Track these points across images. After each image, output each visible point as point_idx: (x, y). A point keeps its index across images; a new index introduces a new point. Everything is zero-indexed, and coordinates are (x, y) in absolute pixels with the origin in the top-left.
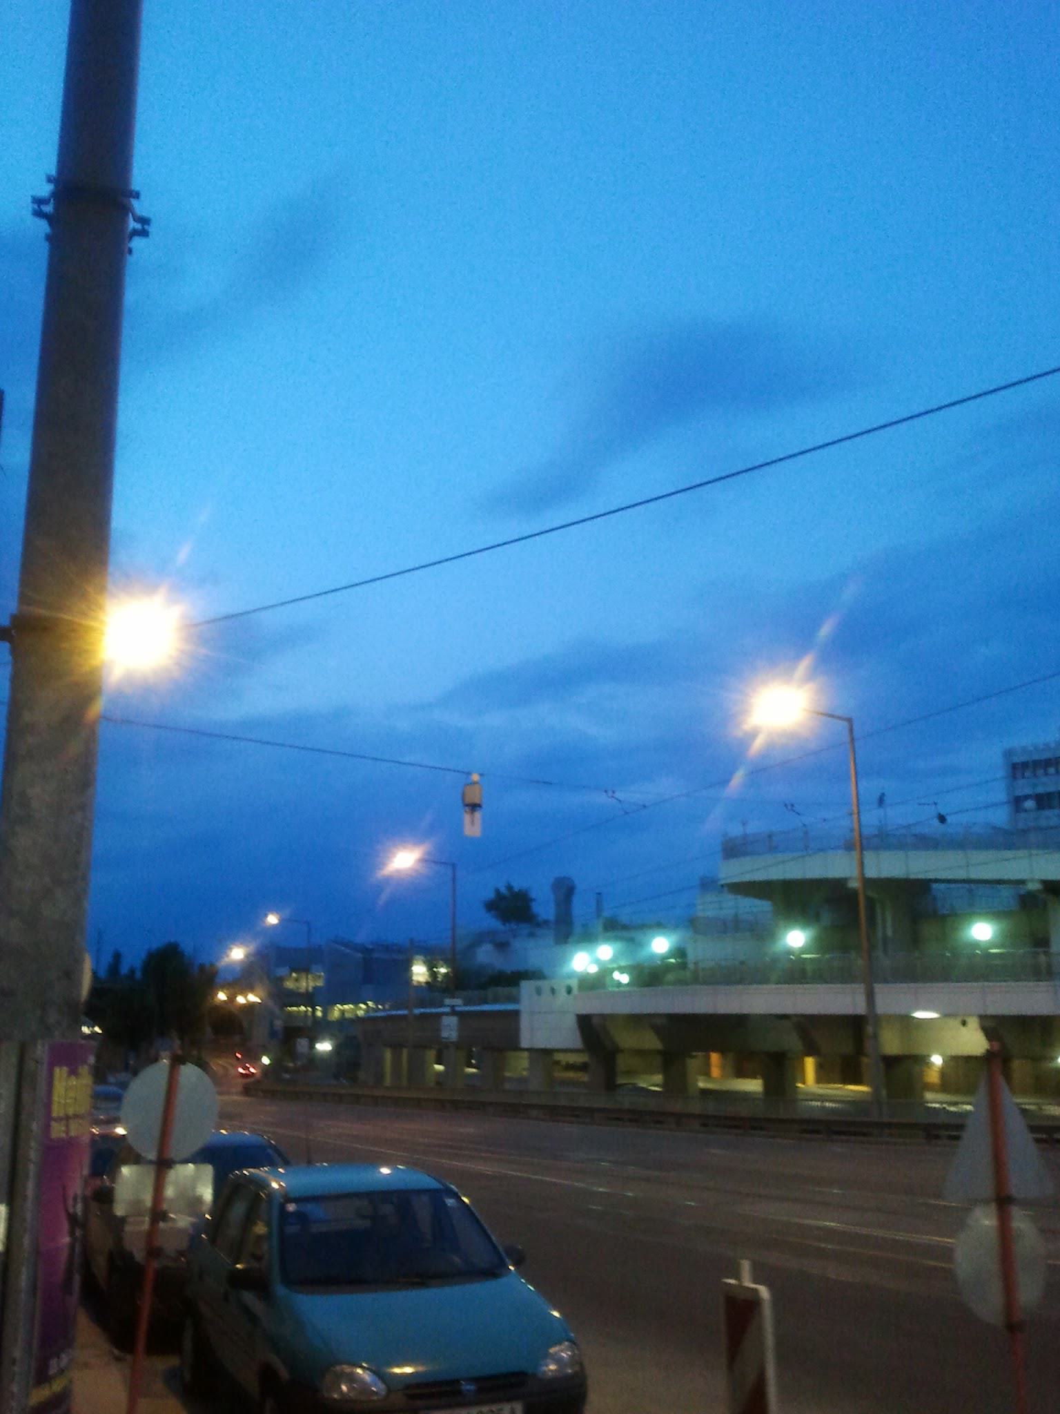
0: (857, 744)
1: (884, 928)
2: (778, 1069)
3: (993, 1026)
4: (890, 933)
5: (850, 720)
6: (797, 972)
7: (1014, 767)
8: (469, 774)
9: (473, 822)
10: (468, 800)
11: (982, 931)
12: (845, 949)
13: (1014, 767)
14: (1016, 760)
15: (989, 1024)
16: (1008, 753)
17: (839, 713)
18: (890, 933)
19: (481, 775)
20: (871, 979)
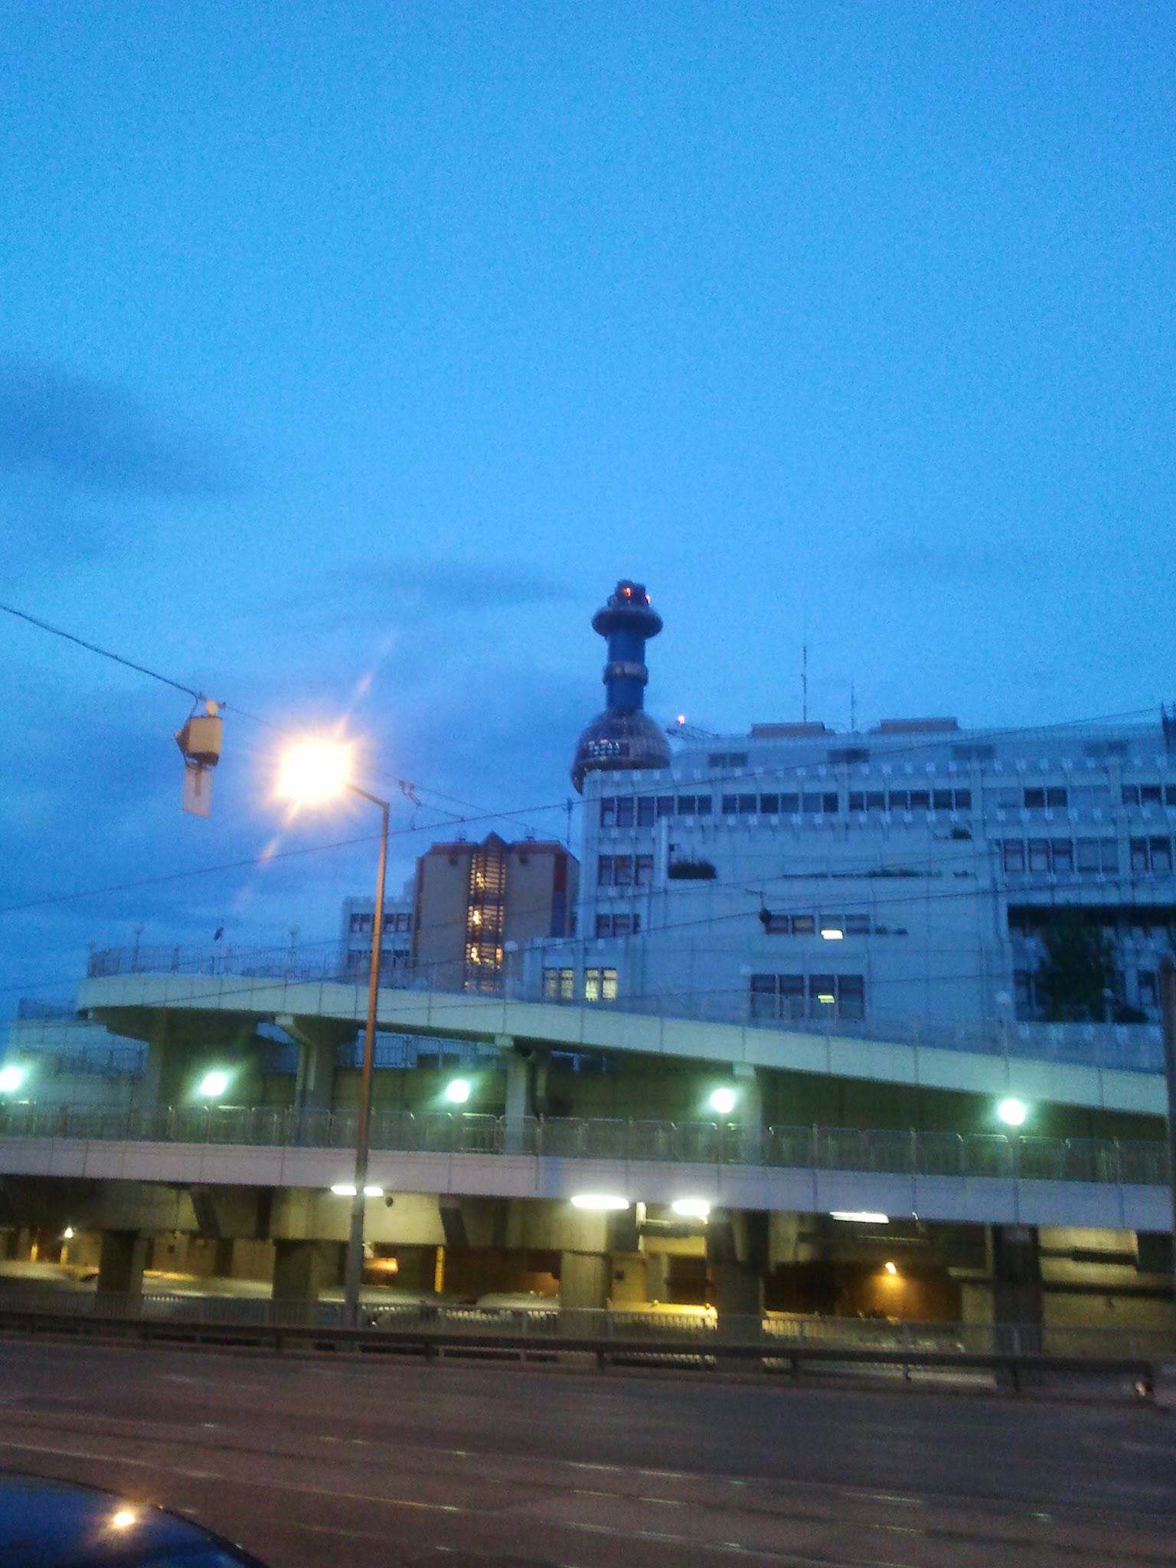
0: (391, 840)
1: (305, 1079)
2: (125, 1251)
3: (456, 1212)
4: (311, 1086)
5: (386, 806)
6: (218, 1129)
7: (354, 918)
8: (200, 697)
9: (198, 792)
10: (196, 744)
11: (458, 1091)
12: (263, 1101)
13: (354, 918)
14: (356, 911)
15: (451, 1205)
16: (349, 903)
17: (380, 797)
18: (311, 1086)
19: (222, 706)
20: (542, 1148)
